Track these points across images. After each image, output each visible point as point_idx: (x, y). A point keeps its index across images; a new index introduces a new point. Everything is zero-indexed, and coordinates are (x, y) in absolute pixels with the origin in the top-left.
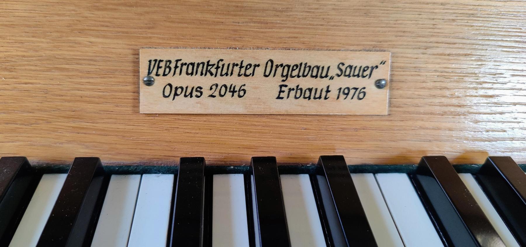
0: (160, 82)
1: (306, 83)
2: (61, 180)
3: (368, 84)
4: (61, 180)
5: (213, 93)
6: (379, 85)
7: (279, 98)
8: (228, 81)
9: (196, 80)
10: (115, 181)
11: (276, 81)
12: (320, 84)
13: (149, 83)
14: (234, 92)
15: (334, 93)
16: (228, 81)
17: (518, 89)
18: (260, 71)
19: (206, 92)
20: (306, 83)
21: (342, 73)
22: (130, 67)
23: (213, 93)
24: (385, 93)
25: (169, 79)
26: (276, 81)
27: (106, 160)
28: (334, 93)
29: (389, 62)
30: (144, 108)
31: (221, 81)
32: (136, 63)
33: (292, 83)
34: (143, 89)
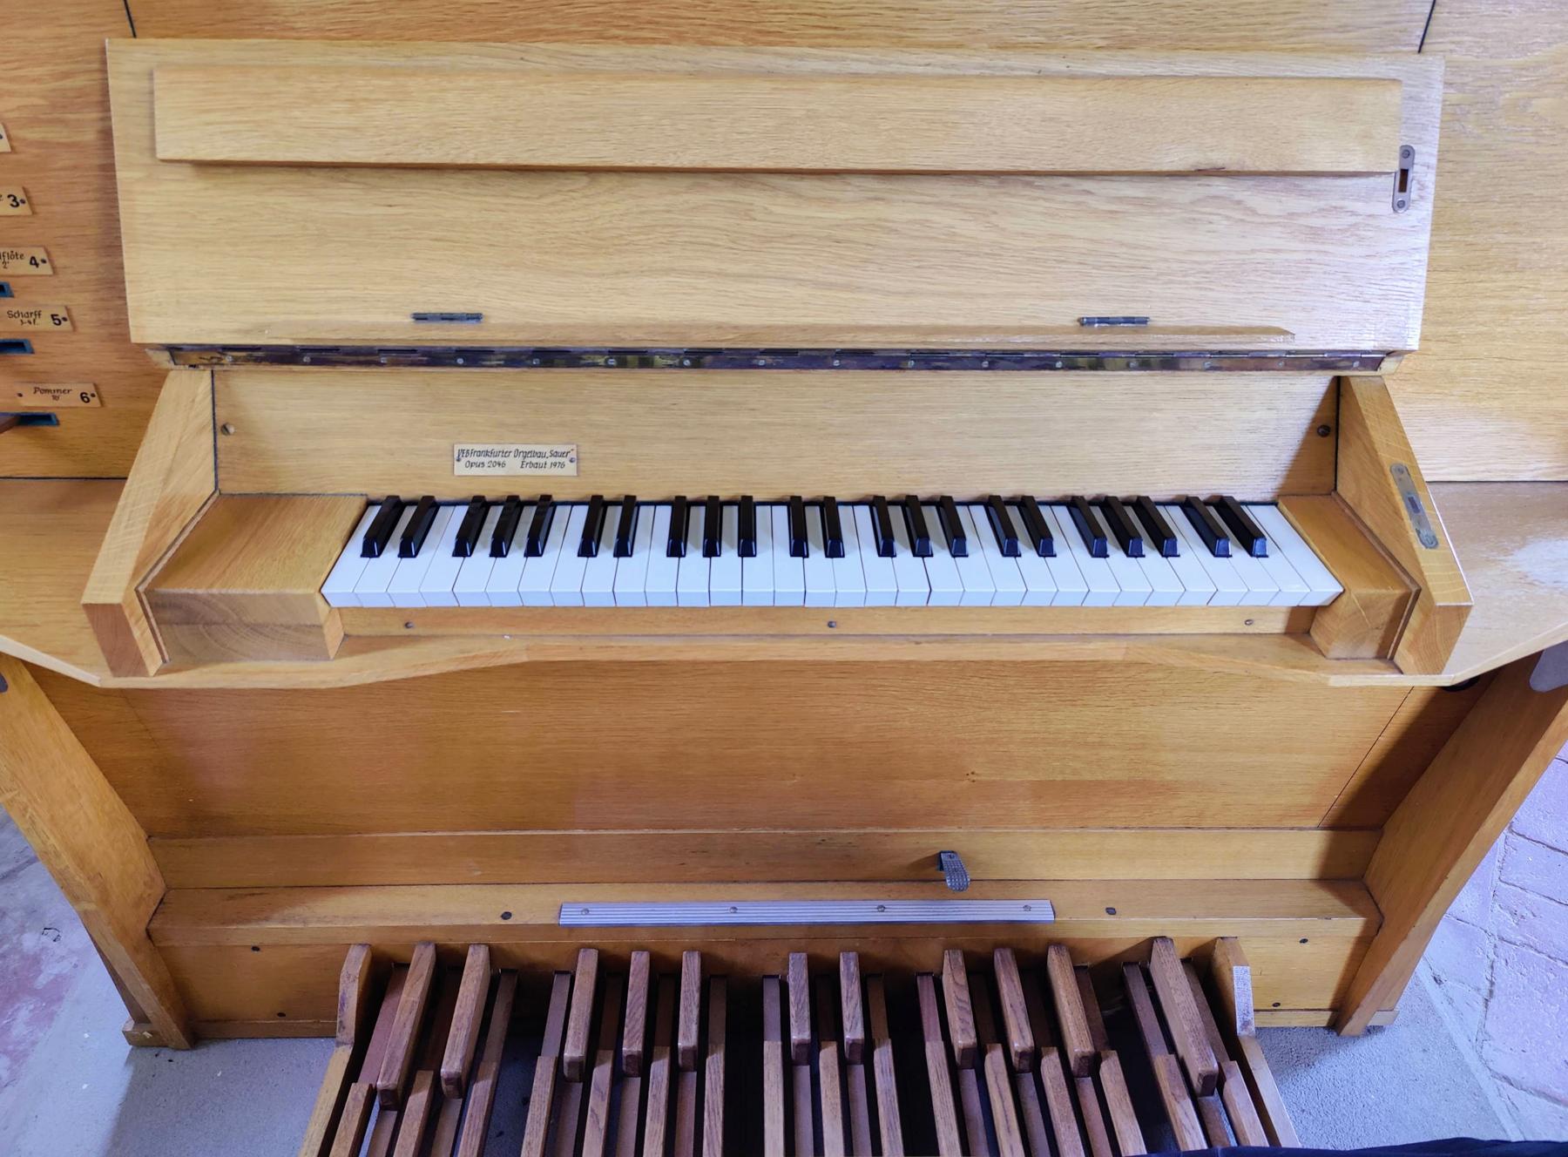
0: (464, 460)
1: (535, 460)
2: (500, 509)
3: (565, 460)
4: (500, 509)
5: (1178, 601)
6: (571, 461)
7: (522, 467)
8: (497, 459)
9: (482, 459)
10: (442, 509)
11: (520, 459)
12: (542, 461)
13: (458, 460)
14: (499, 464)
15: (548, 465)
16: (497, 459)
17: (468, 319)
18: (512, 454)
19: (486, 465)
20: (535, 460)
21: (552, 455)
22: (450, 453)
23: (1178, 601)
24: (574, 464)
25: (468, 459)
26: (520, 459)
27: (438, 498)
28: (548, 465)
29: (575, 448)
30: (456, 473)
31: (493, 459)
32: (453, 451)
33: (528, 460)
34: (456, 462)
